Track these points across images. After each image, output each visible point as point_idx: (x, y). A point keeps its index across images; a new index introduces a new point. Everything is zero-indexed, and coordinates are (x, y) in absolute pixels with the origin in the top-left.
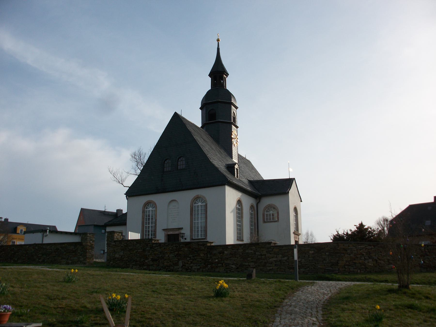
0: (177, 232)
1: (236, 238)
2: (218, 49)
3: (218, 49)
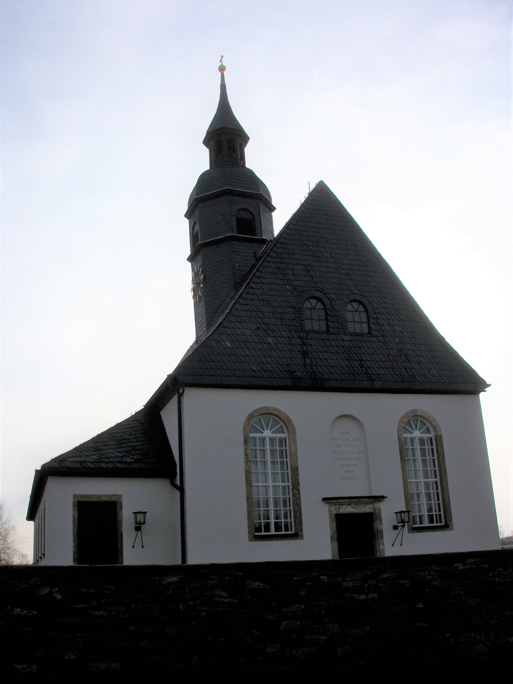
0: (367, 509)
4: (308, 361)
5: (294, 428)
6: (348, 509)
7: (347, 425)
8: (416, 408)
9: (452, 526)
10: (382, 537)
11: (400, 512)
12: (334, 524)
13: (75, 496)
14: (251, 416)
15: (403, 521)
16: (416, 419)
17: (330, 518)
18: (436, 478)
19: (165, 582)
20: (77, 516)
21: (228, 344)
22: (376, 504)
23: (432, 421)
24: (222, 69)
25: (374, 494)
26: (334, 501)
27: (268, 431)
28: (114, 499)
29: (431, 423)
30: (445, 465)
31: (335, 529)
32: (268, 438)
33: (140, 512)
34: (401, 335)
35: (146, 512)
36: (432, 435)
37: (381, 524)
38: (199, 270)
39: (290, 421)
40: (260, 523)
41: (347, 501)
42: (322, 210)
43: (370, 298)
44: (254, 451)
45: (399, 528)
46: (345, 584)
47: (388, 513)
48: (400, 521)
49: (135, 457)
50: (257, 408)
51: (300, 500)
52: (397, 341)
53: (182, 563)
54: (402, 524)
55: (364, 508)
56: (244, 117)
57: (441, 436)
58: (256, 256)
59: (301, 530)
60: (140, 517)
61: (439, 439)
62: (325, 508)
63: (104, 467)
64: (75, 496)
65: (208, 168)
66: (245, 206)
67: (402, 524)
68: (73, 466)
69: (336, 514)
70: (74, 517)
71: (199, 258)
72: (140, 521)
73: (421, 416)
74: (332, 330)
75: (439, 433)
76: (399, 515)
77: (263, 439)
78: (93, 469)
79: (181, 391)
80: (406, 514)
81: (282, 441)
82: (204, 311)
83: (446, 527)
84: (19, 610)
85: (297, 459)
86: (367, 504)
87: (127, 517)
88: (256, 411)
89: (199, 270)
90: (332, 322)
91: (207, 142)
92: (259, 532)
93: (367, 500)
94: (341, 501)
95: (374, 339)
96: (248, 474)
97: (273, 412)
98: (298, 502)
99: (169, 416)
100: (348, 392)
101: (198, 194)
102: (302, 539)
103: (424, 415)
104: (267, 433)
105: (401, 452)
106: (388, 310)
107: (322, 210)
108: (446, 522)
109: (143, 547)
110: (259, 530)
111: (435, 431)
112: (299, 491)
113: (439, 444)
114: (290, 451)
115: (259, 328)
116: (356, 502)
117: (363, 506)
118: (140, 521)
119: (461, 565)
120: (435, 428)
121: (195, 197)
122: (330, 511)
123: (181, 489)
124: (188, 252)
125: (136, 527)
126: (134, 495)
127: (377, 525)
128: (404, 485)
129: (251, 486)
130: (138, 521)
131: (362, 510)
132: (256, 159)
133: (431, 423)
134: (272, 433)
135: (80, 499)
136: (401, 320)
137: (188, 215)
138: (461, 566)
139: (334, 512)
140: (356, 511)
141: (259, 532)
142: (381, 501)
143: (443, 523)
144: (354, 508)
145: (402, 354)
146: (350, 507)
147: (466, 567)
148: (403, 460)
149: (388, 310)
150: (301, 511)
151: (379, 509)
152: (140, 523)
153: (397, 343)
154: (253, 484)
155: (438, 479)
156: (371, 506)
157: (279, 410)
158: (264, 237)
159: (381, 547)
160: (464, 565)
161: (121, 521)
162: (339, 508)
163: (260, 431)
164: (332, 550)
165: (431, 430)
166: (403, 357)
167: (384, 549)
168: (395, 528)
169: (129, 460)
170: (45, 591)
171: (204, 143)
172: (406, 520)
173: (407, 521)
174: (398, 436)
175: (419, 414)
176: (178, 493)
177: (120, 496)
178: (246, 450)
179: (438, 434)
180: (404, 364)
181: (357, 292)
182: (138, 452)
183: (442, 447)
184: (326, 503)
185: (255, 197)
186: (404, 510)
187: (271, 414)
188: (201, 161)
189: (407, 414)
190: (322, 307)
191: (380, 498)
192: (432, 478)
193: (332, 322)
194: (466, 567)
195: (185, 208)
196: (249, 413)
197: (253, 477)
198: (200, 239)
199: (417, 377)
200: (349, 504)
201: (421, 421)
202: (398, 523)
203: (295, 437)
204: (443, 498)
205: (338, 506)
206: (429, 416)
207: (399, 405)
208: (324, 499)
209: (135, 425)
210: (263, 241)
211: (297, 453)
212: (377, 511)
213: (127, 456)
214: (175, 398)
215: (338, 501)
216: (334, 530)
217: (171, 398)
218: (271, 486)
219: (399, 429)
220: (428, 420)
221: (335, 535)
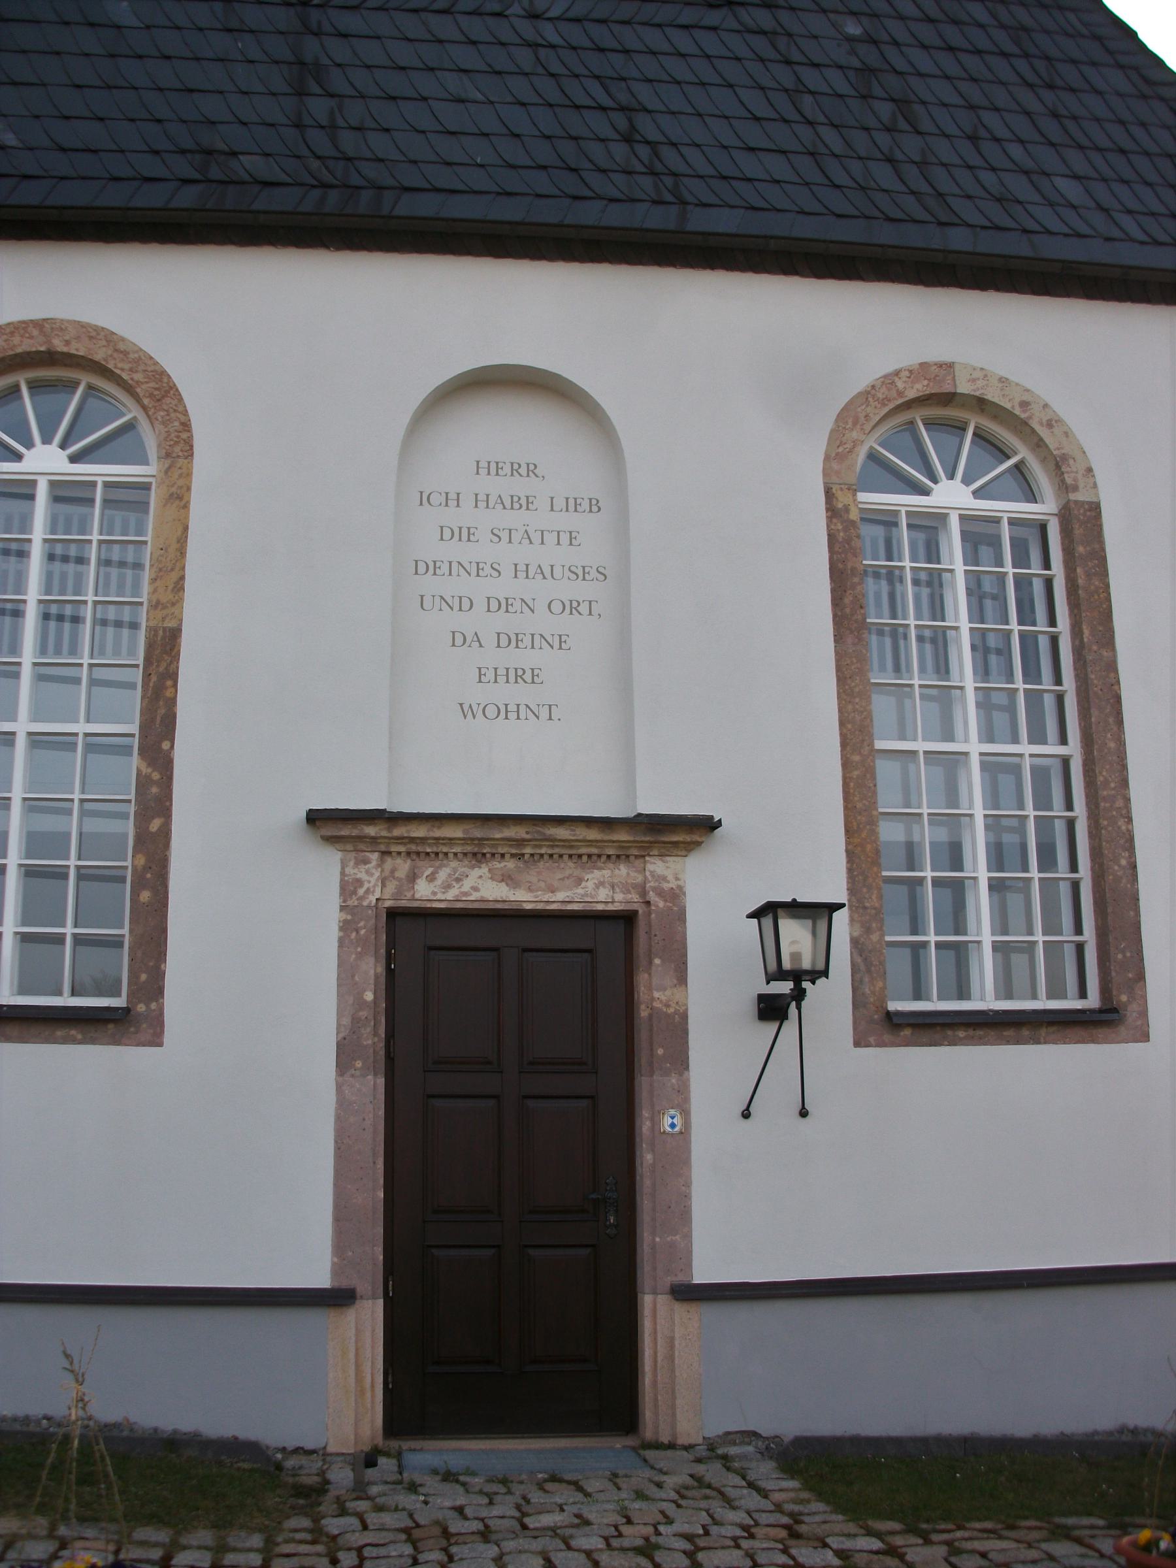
0: (598, 888)
4: (319, 108)
5: (186, 426)
6: (467, 885)
8: (947, 358)
9: (1144, 1013)
10: (681, 1062)
12: (371, 968)
16: (940, 410)
18: (1063, 741)
22: (657, 866)
23: (1043, 432)
26: (371, 830)
27: (54, 448)
29: (1038, 445)
30: (1112, 666)
31: (369, 996)
33: (796, 908)
36: (1045, 508)
37: (682, 980)
41: (454, 831)
52: (853, 29)
55: (579, 881)
61: (1083, 525)
62: (324, 868)
69: (393, 915)
72: (796, 956)
73: (981, 404)
75: (1080, 496)
77: (929, 527)
81: (127, 499)
86: (593, 859)
94: (419, 831)
102: (156, 1040)
103: (992, 395)
104: (952, 496)
105: (843, 578)
108: (1105, 990)
111: (1064, 487)
116: (520, 843)
117: (570, 867)
118: (796, 956)
120: (1057, 465)
122: (348, 888)
125: (762, 998)
127: (654, 991)
128: (846, 764)
130: (787, 964)
131: (561, 896)
133: (1038, 445)
140: (523, 897)
144: (507, 879)
145: (877, 91)
146: (484, 870)
148: (848, 621)
151: (676, 896)
152: (797, 976)
153: (850, 39)
155: (1074, 749)
156: (623, 870)
157: (110, 338)
159: (669, 1121)
162: (413, 878)
164: (338, 1119)
166: (885, 110)
167: (685, 1133)
174: (829, 494)
175: (963, 388)
179: (1073, 497)
180: (883, 139)
189: (889, 379)
191: (693, 831)
192: (1037, 737)
199: (957, 204)
200: (478, 857)
201: (929, 424)
203: (189, 475)
204: (1096, 854)
205: (403, 867)
206: (1024, 405)
208: (315, 818)
211: (182, 552)
215: (399, 831)
216: (362, 1004)
220: (1021, 427)
221: (373, 1039)
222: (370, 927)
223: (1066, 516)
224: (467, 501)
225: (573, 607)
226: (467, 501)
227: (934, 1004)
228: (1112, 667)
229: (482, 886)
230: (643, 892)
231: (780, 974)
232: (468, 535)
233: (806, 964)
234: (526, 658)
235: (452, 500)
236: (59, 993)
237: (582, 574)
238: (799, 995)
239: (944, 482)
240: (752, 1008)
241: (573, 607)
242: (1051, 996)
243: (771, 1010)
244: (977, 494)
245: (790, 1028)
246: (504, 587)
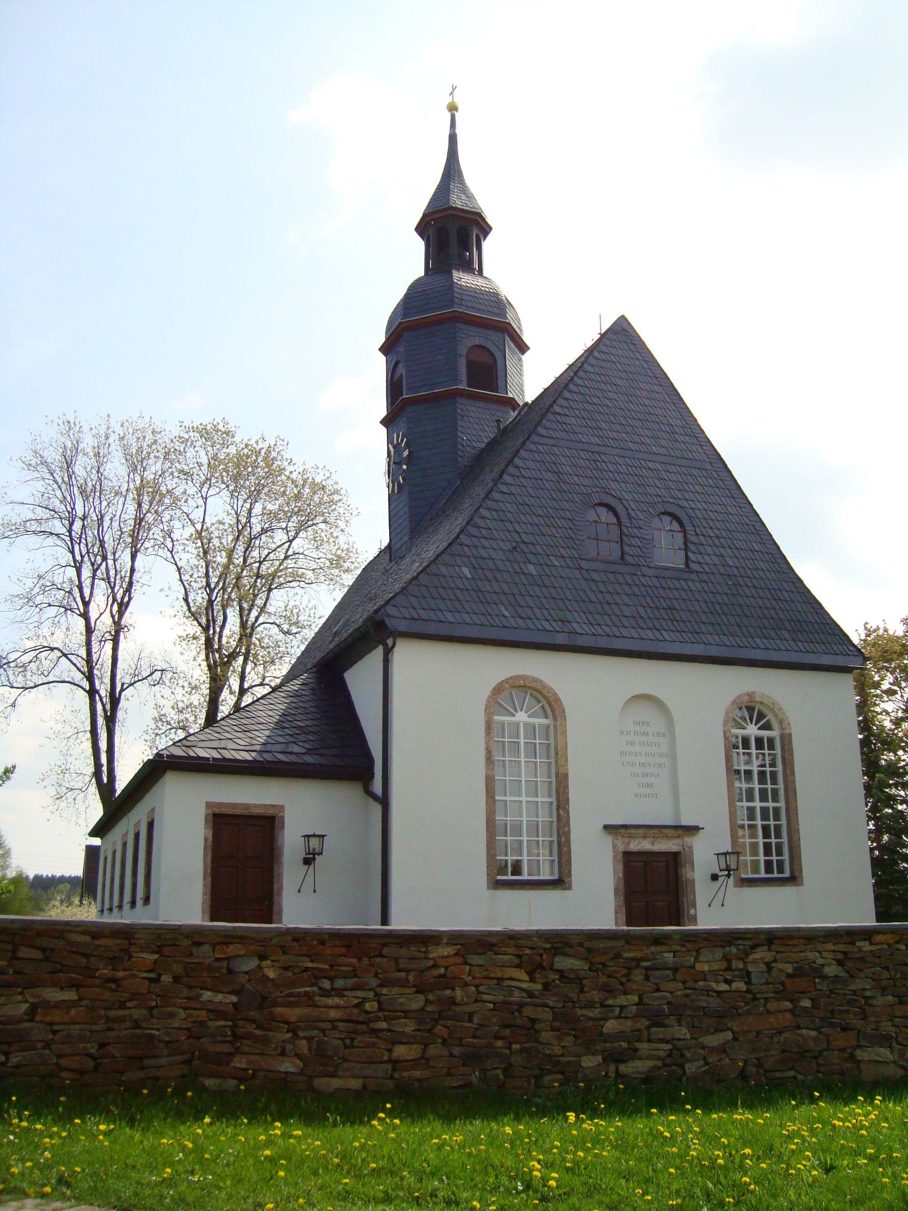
1: (224, 810)
2: (453, 139)
3: (453, 139)
5: (564, 710)
7: (647, 713)
11: (725, 854)
12: (620, 867)
13: (209, 805)
14: (498, 690)
15: (728, 869)
16: (753, 710)
17: (615, 857)
19: (435, 955)
20: (210, 839)
21: (466, 571)
22: (687, 840)
24: (453, 108)
25: (684, 823)
27: (523, 713)
28: (271, 812)
29: (776, 715)
30: (794, 782)
31: (621, 875)
32: (522, 725)
33: (314, 836)
34: (736, 571)
35: (323, 836)
37: (693, 870)
38: (402, 441)
39: (558, 700)
40: (506, 861)
41: (641, 831)
42: (618, 358)
43: (690, 511)
44: (500, 744)
45: (721, 879)
46: (698, 967)
47: (704, 854)
48: (724, 866)
49: (306, 745)
50: (508, 676)
51: (569, 826)
53: (218, 906)
54: (726, 873)
56: (484, 191)
57: (790, 735)
58: (499, 425)
59: (569, 875)
60: (314, 843)
61: (786, 740)
63: (269, 759)
64: (209, 805)
65: (421, 272)
66: (482, 342)
67: (726, 873)
68: (207, 756)
69: (624, 852)
70: (206, 840)
71: (402, 425)
72: (314, 849)
74: (628, 558)
75: (787, 731)
76: (722, 858)
78: (314, 765)
79: (390, 642)
80: (734, 857)
82: (406, 509)
83: (794, 879)
84: (209, 993)
85: (566, 760)
87: (291, 841)
88: (506, 681)
89: (402, 441)
90: (630, 546)
91: (422, 229)
92: (505, 876)
93: (673, 831)
94: (633, 831)
95: (693, 576)
96: (490, 782)
97: (533, 685)
98: (566, 829)
99: (361, 682)
100: (624, 656)
101: (405, 315)
103: (766, 701)
104: (521, 717)
106: (717, 532)
107: (618, 358)
109: (315, 891)
110: (502, 870)
112: (567, 812)
113: (787, 748)
114: (556, 747)
115: (515, 548)
118: (314, 849)
119: (867, 943)
121: (399, 321)
122: (614, 846)
123: (384, 802)
124: (382, 411)
125: (304, 858)
126: (305, 809)
127: (686, 872)
129: (494, 801)
132: (502, 265)
133: (776, 715)
134: (759, 729)
135: (217, 811)
136: (737, 548)
137: (385, 349)
138: (865, 946)
139: (621, 848)
141: (505, 876)
142: (694, 835)
143: (787, 874)
147: (873, 948)
149: (717, 532)
150: (569, 843)
151: (691, 847)
152: (314, 854)
154: (497, 798)
156: (678, 841)
158: (510, 395)
160: (871, 944)
161: (281, 849)
162: (629, 843)
163: (509, 712)
165: (775, 724)
168: (715, 877)
169: (296, 749)
170: (251, 964)
171: (416, 229)
172: (733, 866)
173: (729, 869)
176: (377, 809)
177: (282, 807)
178: (487, 743)
181: (671, 500)
182: (311, 737)
183: (792, 754)
184: (610, 833)
185: (493, 331)
186: (730, 851)
187: (530, 688)
188: (410, 261)
190: (615, 521)
191: (693, 830)
193: (630, 546)
194: (873, 948)
195: (381, 339)
196: (495, 684)
197: (498, 787)
198: (404, 390)
200: (644, 837)
202: (721, 870)
205: (626, 840)
206: (773, 704)
207: (729, 684)
208: (606, 827)
209: (303, 692)
210: (511, 403)
212: (687, 849)
213: (294, 743)
214: (379, 651)
217: (371, 650)
218: (524, 803)
219: (725, 723)
220: (772, 710)
221: (622, 887)
222: (620, 856)
223: (782, 737)
224: (632, 734)
225: (660, 765)
226: (632, 734)
227: (776, 875)
228: (794, 782)
229: (645, 845)
230: (683, 846)
231: (310, 854)
232: (633, 744)
233: (317, 851)
234: (650, 780)
235: (628, 733)
236: (507, 875)
237: (661, 755)
238: (314, 859)
239: (520, 713)
240: (302, 861)
241: (660, 765)
242: (753, 873)
243: (308, 861)
244: (529, 716)
245: (312, 866)
246: (643, 759)
